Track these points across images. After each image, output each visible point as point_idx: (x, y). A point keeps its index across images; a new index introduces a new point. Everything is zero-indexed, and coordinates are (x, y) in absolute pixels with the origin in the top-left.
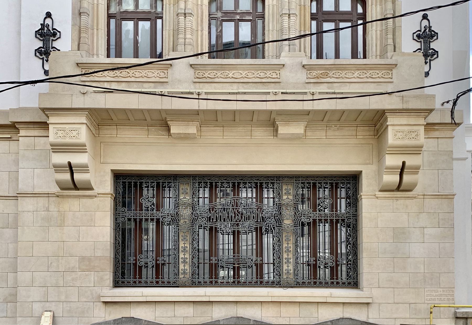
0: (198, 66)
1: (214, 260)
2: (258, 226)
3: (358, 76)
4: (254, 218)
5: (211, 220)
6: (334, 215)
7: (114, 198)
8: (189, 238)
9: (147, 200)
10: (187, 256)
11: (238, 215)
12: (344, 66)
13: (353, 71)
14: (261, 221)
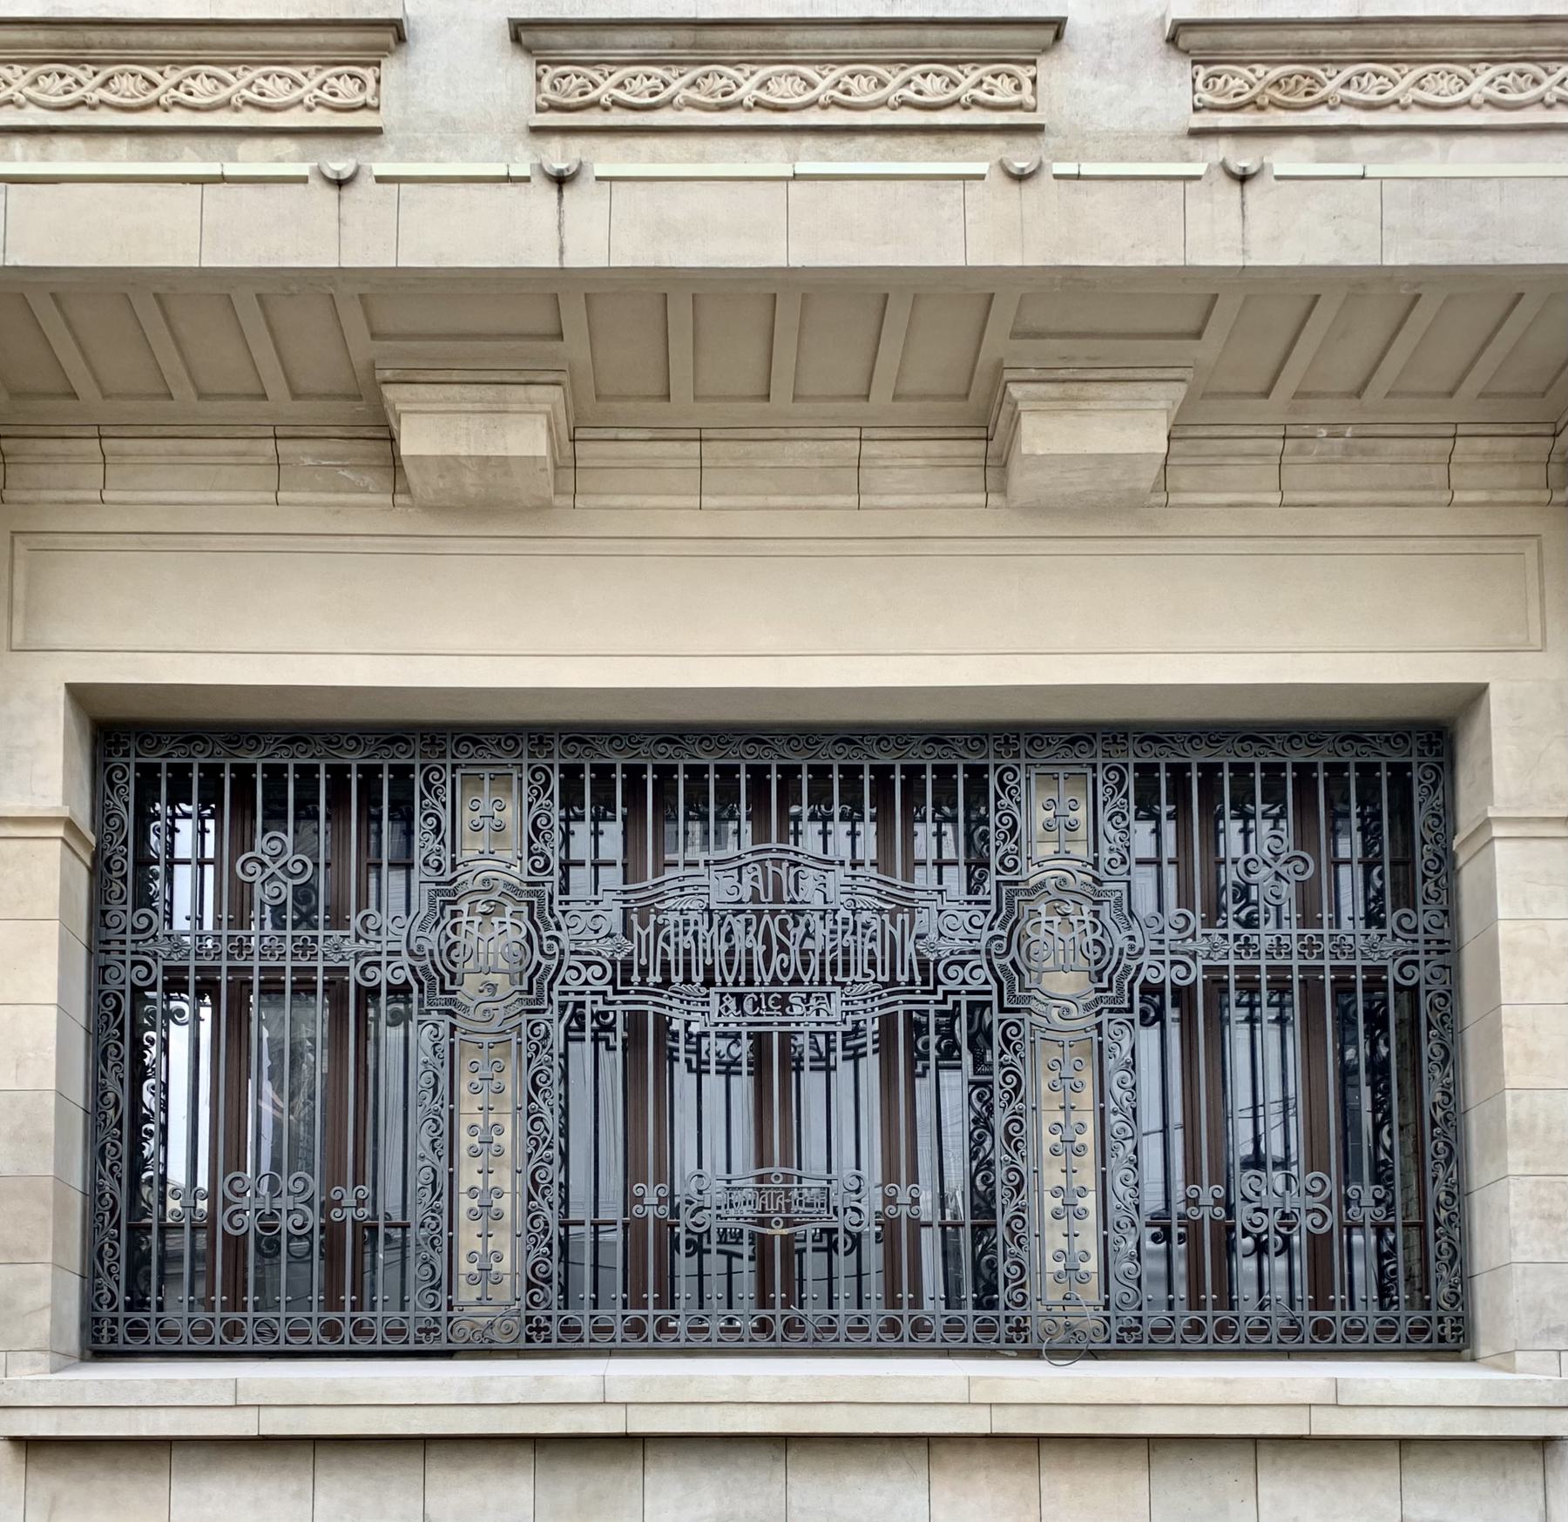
0: (560, 37)
1: (651, 1199)
2: (900, 1009)
3: (1492, 92)
4: (872, 965)
5: (636, 978)
6: (1327, 946)
7: (94, 858)
8: (513, 1082)
9: (273, 868)
10: (503, 1178)
11: (784, 949)
12: (1412, 34)
13: (1463, 70)
14: (912, 982)
